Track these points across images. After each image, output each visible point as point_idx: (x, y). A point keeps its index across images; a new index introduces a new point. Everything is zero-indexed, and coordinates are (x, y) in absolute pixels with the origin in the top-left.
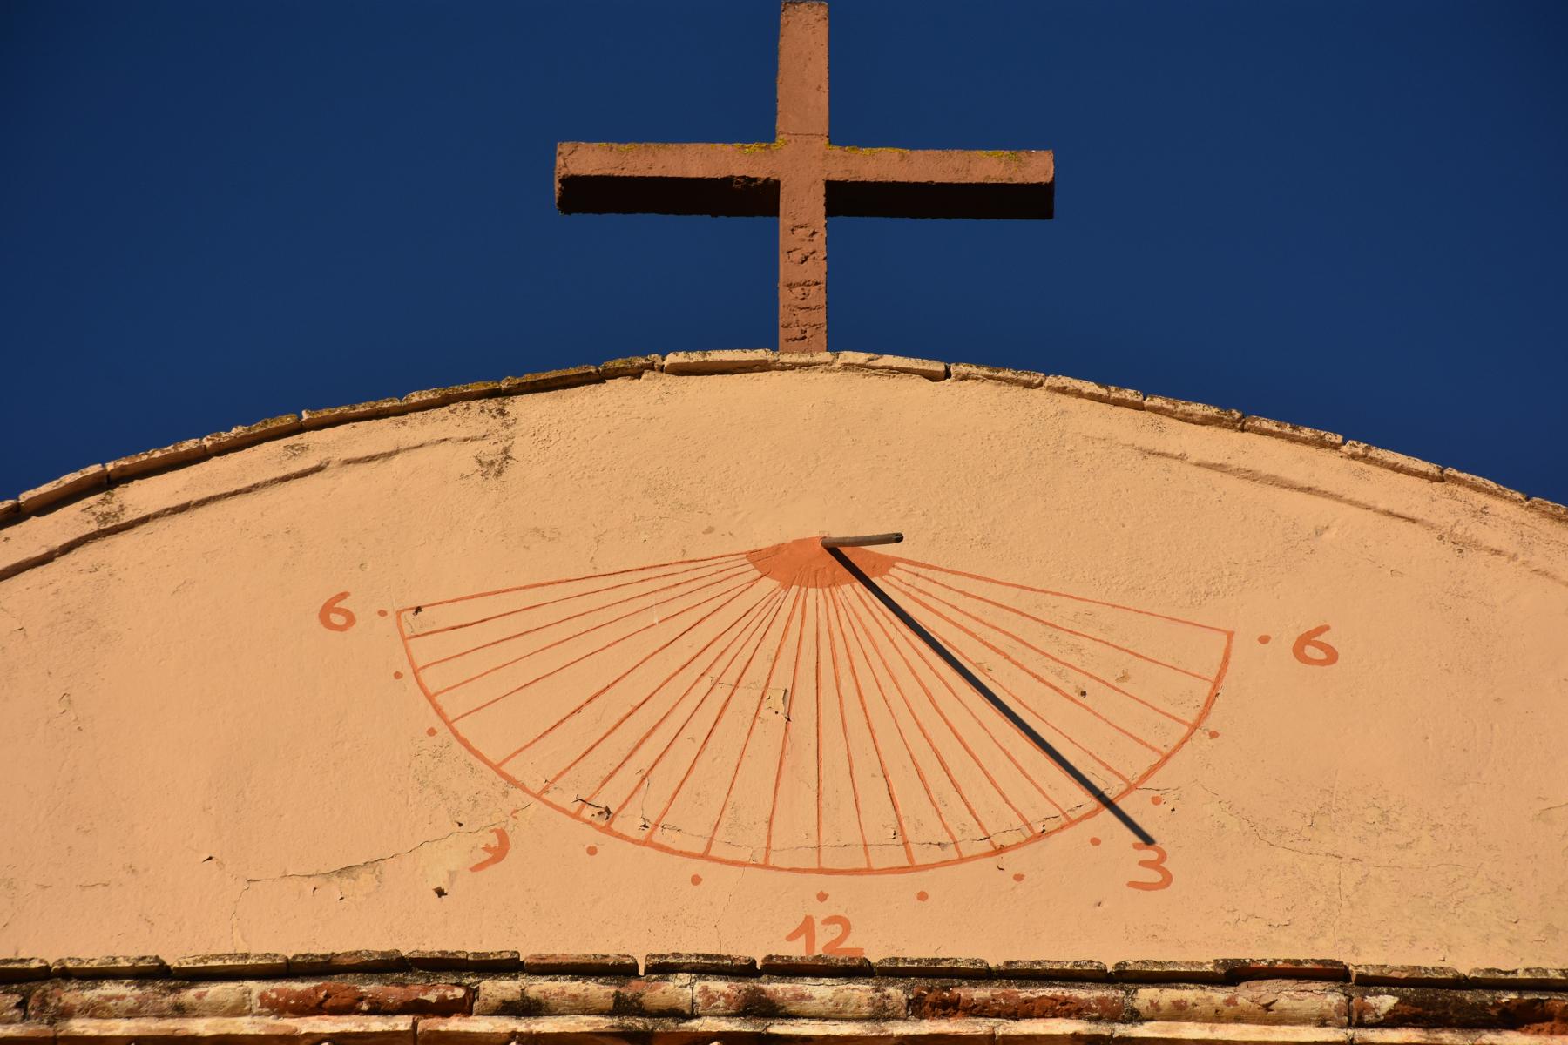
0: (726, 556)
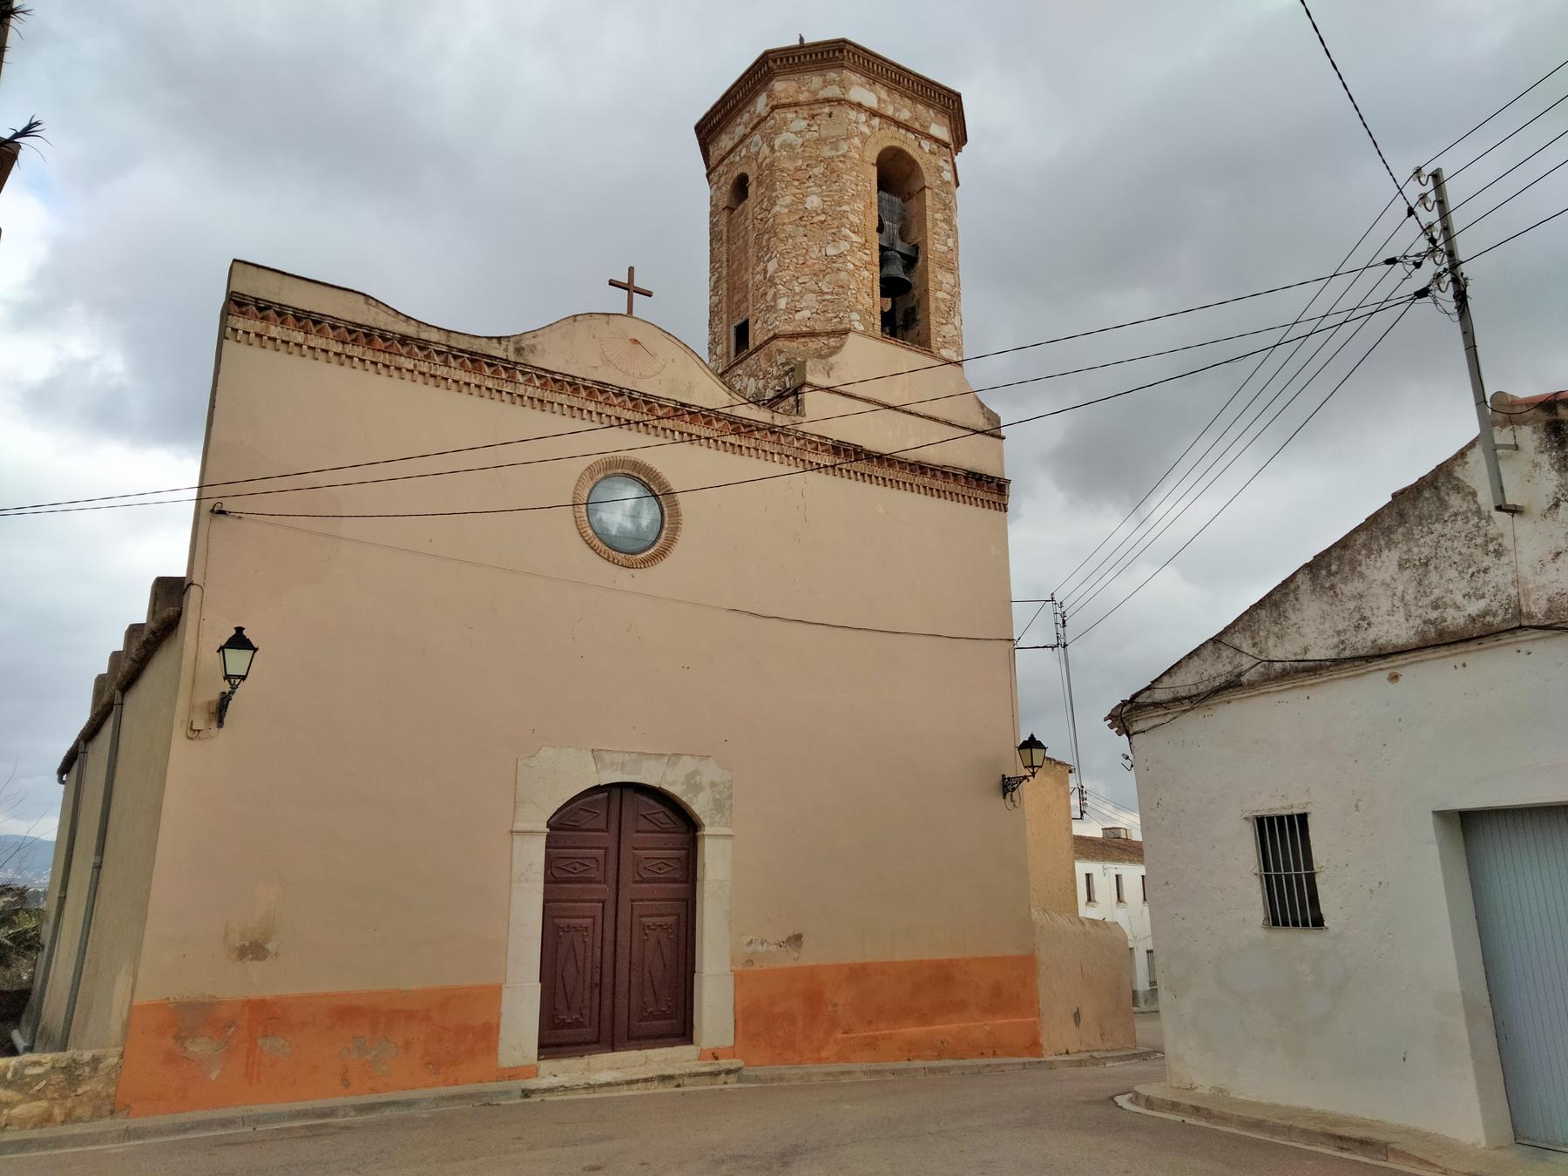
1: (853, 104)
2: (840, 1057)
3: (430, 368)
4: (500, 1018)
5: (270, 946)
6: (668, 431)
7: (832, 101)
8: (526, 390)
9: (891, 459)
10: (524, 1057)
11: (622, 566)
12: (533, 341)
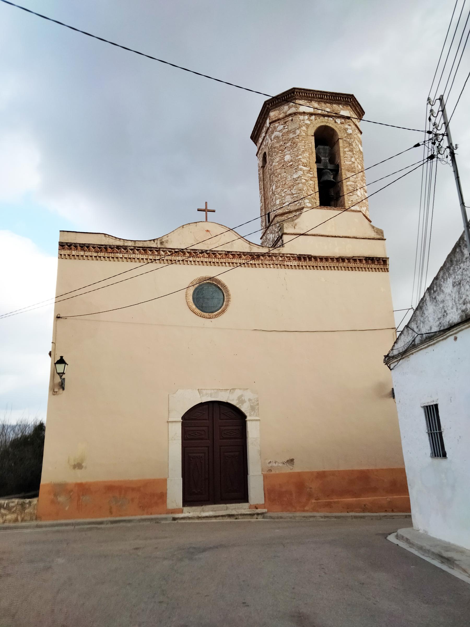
1: (301, 113)
2: (314, 510)
3: (128, 256)
4: (167, 491)
5: (84, 464)
6: (223, 263)
7: (292, 115)
9: (326, 258)
10: (177, 505)
11: (207, 318)
12: (167, 239)
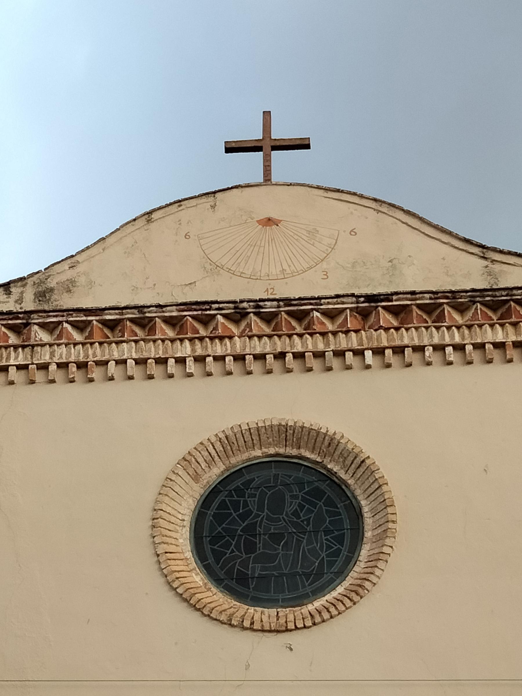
0: (342, 192)
8: (52, 354)
11: (263, 631)
12: (70, 274)
